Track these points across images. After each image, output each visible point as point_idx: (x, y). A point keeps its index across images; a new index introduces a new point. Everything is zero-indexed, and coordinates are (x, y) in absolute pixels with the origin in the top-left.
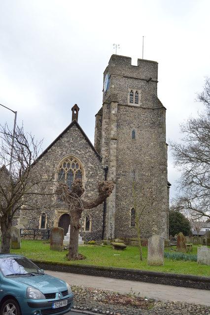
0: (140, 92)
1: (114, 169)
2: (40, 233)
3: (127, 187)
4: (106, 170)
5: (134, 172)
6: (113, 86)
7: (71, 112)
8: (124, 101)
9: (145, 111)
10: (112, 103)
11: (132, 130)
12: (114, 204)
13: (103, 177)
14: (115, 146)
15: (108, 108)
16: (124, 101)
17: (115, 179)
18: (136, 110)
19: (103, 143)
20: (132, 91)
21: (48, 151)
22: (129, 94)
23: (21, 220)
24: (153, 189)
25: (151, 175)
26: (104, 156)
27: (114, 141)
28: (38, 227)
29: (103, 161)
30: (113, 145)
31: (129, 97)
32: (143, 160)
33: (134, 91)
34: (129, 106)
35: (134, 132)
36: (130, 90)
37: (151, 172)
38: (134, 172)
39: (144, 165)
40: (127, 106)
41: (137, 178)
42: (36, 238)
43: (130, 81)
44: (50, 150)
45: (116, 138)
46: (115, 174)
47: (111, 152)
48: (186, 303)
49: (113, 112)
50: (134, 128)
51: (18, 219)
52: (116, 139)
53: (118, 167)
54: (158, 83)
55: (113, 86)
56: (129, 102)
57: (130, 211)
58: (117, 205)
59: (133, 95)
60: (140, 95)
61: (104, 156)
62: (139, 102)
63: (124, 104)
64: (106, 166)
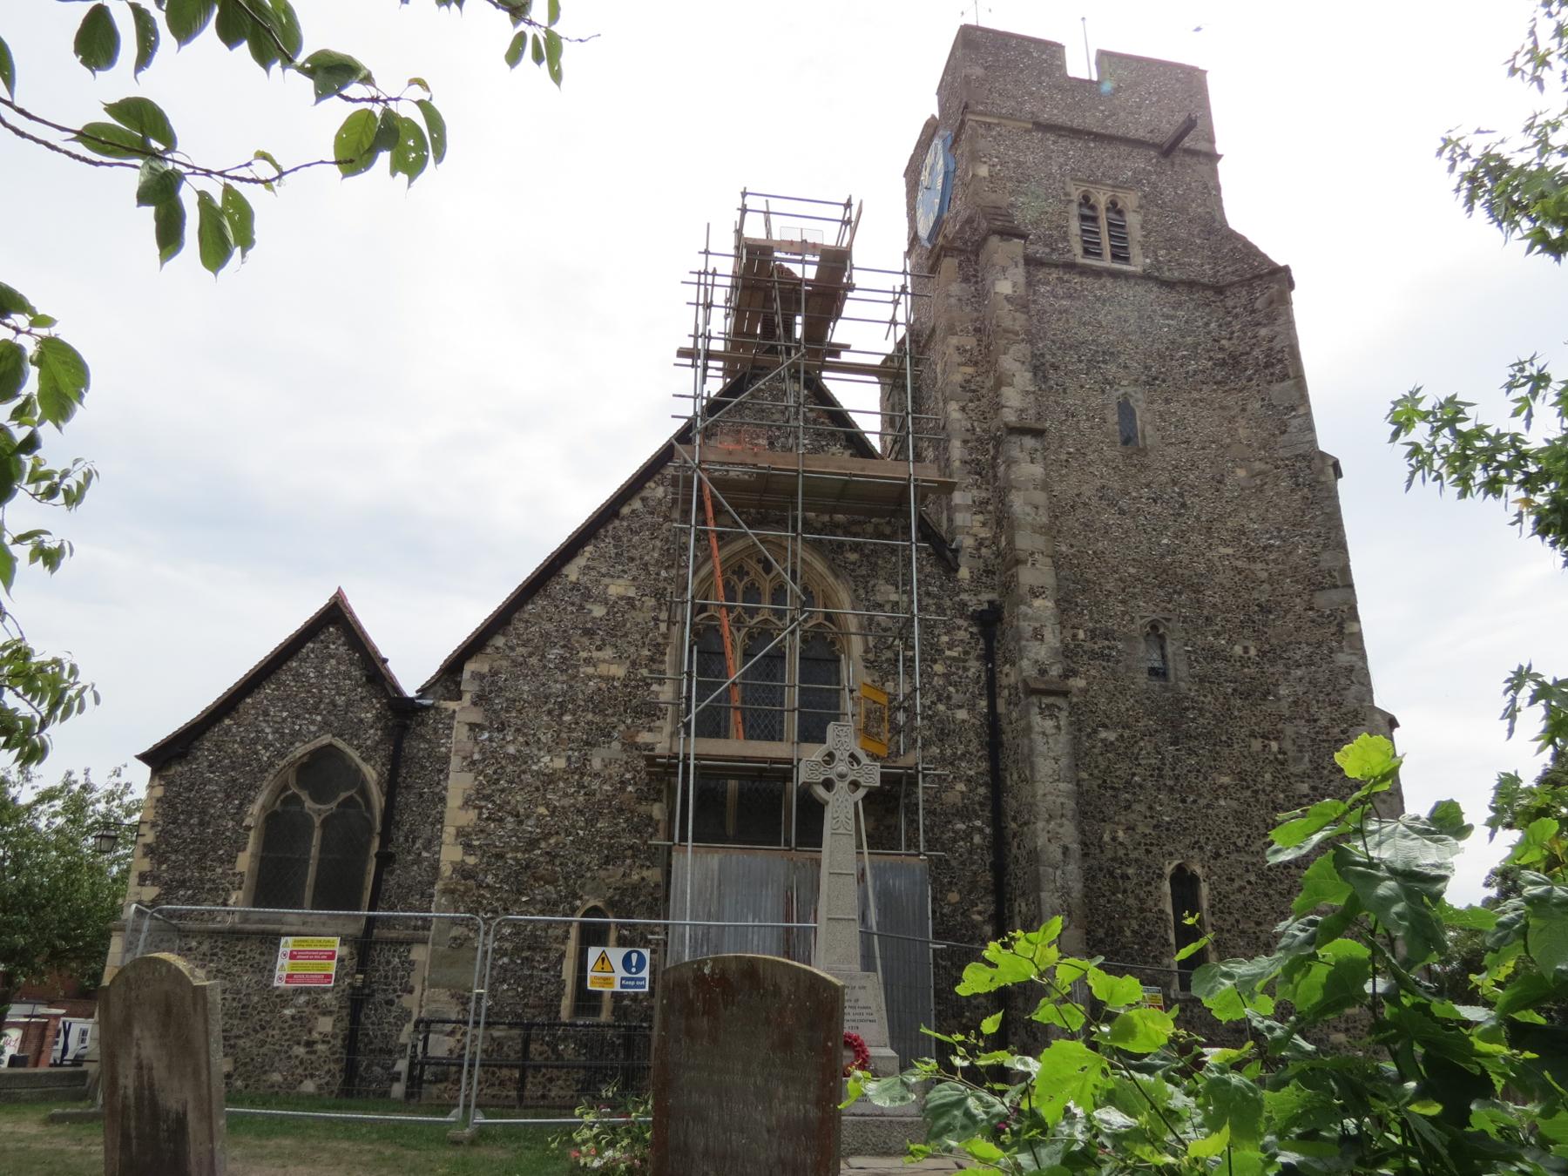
0: (1130, 200)
1: (1044, 606)
2: (568, 1049)
3: (1126, 726)
4: (990, 623)
5: (1155, 634)
6: (983, 171)
7: (49, 659)
8: (1050, 243)
9: (1173, 297)
10: (994, 241)
11: (1115, 395)
12: (1069, 832)
13: (974, 667)
14: (1037, 470)
15: (966, 280)
16: (1050, 243)
17: (1055, 671)
18: (1126, 291)
19: (957, 463)
20: (1086, 198)
21: (625, 510)
22: (1074, 210)
23: (437, 962)
24: (1288, 745)
25: (1262, 654)
26: (969, 542)
27: (1029, 442)
28: (552, 1006)
29: (964, 573)
30: (1026, 467)
31: (1075, 226)
32: (1202, 568)
33: (1101, 199)
34: (1084, 271)
35: (1126, 410)
36: (1076, 195)
37: (1258, 634)
38: (1155, 634)
39: (1211, 597)
40: (1071, 266)
41: (1179, 669)
42: (532, 1090)
43: (1074, 150)
44: (637, 504)
45: (1031, 422)
46: (1052, 638)
47: (1018, 503)
48: (1165, 576)
49: (1004, 287)
50: (1125, 387)
51: (419, 954)
52: (1038, 433)
53: (1065, 605)
54: (1220, 165)
55: (983, 171)
56: (1078, 249)
57: (1166, 887)
58: (1088, 846)
59: (1094, 219)
60: (1133, 220)
61: (969, 542)
62: (1135, 251)
63: (1063, 259)
64: (986, 596)
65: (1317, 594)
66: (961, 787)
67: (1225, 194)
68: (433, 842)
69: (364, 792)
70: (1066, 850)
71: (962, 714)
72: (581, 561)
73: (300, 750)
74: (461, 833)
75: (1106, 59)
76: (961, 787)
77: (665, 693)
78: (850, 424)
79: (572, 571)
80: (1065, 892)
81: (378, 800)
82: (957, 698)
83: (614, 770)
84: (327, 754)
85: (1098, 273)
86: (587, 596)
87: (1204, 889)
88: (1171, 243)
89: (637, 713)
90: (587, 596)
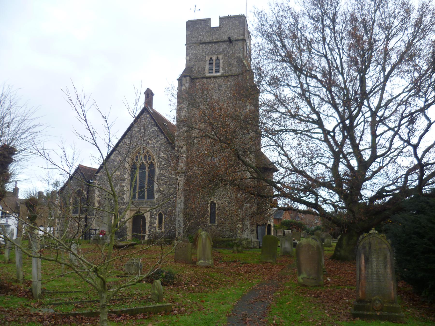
0: (220, 57)
21: (120, 145)
22: (208, 62)
33: (214, 58)
34: (210, 78)
44: (121, 143)
65: (408, 131)
66: (173, 189)
67: (184, 41)
68: (94, 203)
69: (85, 196)
70: (181, 201)
71: (174, 176)
72: (113, 155)
73: (76, 190)
74: (97, 201)
75: (222, 19)
76: (173, 189)
77: (126, 176)
78: (133, 122)
79: (112, 157)
80: (181, 208)
81: (86, 196)
82: (173, 173)
83: (119, 190)
84: (80, 190)
85: (214, 77)
86: (114, 161)
87: (216, 205)
88: (230, 65)
89: (122, 180)
90: (114, 161)
